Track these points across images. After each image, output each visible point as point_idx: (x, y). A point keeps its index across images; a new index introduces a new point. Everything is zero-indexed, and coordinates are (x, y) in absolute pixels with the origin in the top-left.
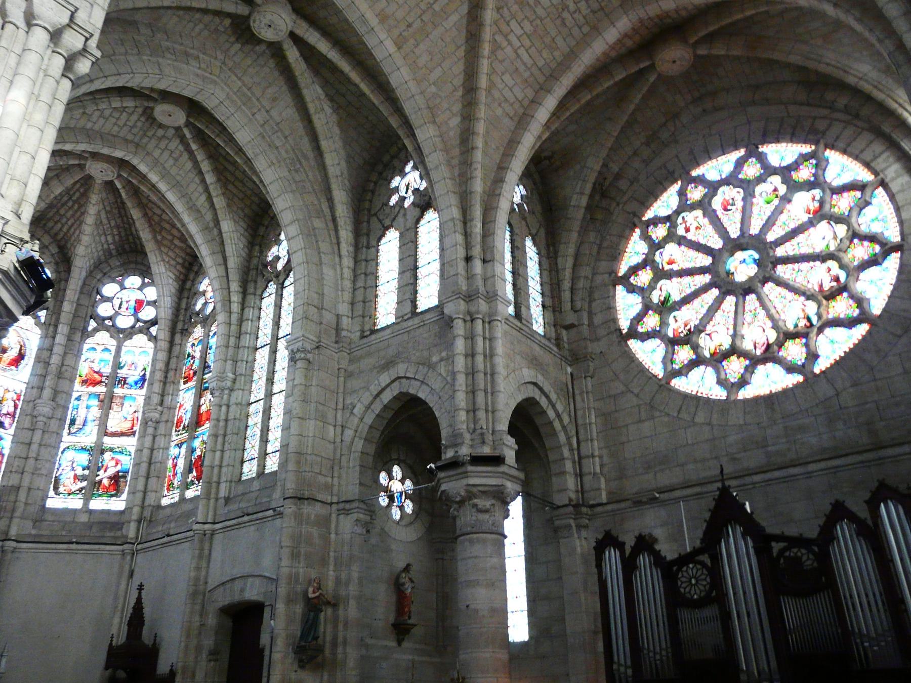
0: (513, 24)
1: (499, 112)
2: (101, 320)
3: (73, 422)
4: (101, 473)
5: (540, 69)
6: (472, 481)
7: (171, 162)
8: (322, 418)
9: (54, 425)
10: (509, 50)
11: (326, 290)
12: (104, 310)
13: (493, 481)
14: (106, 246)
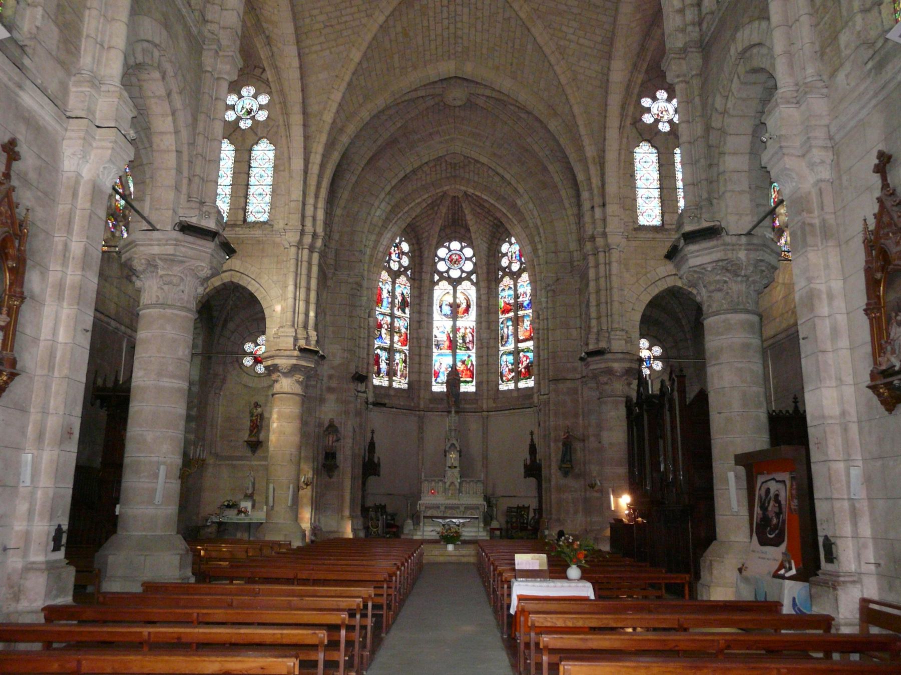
0: (564, 28)
3: (502, 337)
6: (595, 367)
7: (476, 176)
9: (492, 343)
10: (572, 46)
12: (505, 262)
13: (603, 366)
14: (491, 223)
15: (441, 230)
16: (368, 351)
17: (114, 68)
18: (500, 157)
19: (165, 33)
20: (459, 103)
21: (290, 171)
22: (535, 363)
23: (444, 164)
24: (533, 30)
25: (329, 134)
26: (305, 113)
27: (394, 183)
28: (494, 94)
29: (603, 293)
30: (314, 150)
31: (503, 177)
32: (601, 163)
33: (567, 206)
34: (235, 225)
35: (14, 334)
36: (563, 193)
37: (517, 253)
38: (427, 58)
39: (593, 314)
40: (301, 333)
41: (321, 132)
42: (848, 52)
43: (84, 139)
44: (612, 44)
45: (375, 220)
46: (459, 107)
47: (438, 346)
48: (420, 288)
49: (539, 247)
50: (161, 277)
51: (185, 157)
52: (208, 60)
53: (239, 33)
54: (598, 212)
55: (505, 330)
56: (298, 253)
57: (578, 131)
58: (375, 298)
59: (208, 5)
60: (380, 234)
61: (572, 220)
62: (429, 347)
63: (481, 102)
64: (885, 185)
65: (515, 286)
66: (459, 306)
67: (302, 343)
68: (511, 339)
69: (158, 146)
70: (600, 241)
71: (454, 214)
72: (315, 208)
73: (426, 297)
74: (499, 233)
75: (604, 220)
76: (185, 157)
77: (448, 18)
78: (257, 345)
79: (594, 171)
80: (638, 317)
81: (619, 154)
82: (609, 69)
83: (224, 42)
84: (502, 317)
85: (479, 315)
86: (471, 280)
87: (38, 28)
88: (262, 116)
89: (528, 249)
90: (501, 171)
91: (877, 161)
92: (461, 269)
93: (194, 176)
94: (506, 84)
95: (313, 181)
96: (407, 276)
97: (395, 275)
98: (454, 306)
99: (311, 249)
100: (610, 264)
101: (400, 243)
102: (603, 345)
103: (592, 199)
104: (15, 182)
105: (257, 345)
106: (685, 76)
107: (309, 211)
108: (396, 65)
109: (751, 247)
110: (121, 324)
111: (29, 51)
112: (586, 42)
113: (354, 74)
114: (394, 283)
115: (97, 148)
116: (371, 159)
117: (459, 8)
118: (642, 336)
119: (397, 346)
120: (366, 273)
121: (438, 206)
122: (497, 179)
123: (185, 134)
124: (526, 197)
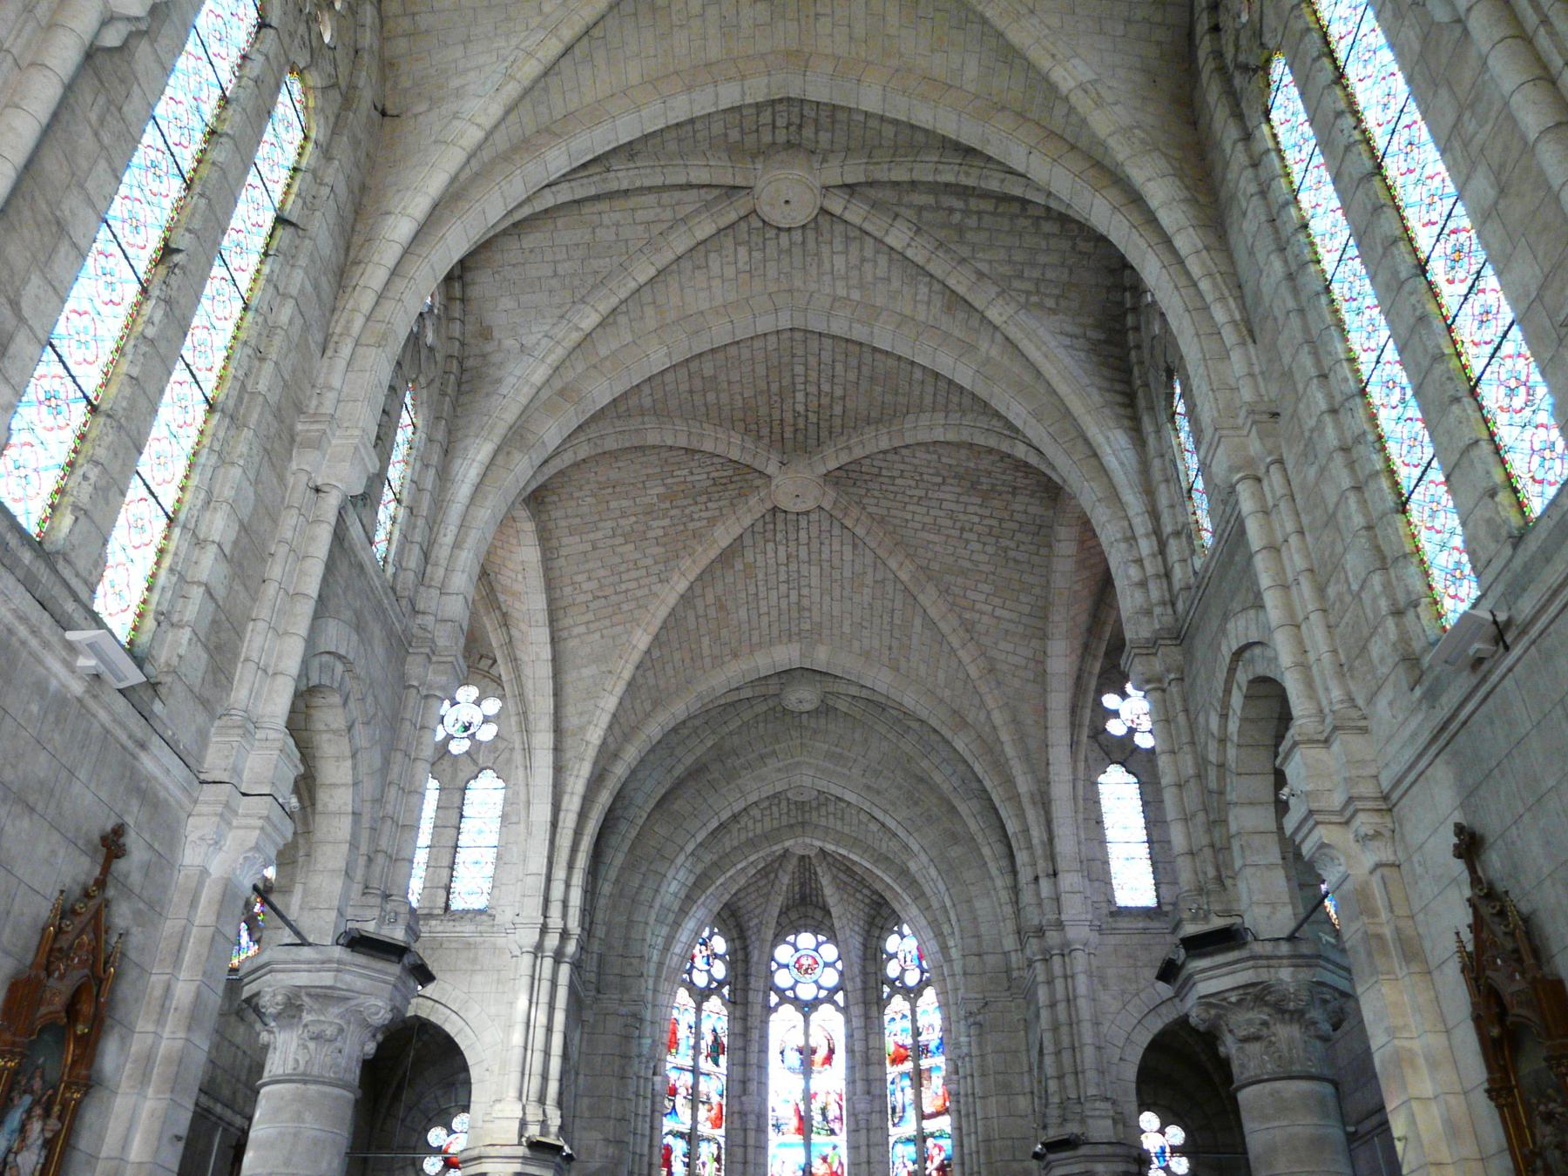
1: (1017, 683)
2: (891, 983)
3: (894, 1109)
4: (928, 1164)
7: (839, 823)
8: (1005, 1089)
9: (875, 1118)
10: (985, 619)
11: (983, 929)
12: (892, 970)
16: (651, 1140)
17: (279, 704)
19: (355, 637)
20: (807, 707)
21: (528, 825)
22: (956, 1160)
23: (784, 803)
24: (921, 598)
25: (595, 763)
26: (558, 730)
28: (865, 693)
29: (1064, 1030)
30: (569, 789)
31: (883, 825)
33: (994, 872)
35: (62, 1153)
36: (986, 851)
37: (915, 952)
38: (755, 639)
39: (1050, 1070)
40: (534, 1113)
42: (1385, 670)
43: (221, 815)
47: (777, 1127)
48: (745, 1019)
49: (951, 943)
50: (306, 1026)
51: (366, 822)
53: (465, 627)
54: (1045, 884)
55: (899, 1094)
58: (666, 1038)
59: (422, 589)
60: (677, 925)
61: (1004, 896)
62: (761, 1130)
63: (842, 705)
64: (1475, 881)
65: (913, 1012)
66: (814, 1052)
67: (533, 1131)
68: (911, 1114)
69: (325, 805)
70: (1053, 937)
71: (802, 885)
72: (568, 885)
73: (755, 1035)
74: (880, 917)
76: (366, 822)
77: (788, 582)
78: (451, 1131)
80: (1131, 1072)
83: (441, 642)
84: (892, 1071)
85: (851, 1068)
86: (835, 1003)
87: (180, 657)
88: (487, 733)
89: (932, 946)
91: (1455, 840)
92: (816, 982)
93: (377, 851)
94: (881, 680)
95: (565, 841)
96: (722, 997)
97: (701, 996)
98: (807, 1053)
99: (558, 957)
101: (710, 938)
102: (1073, 1128)
103: (1034, 864)
104: (111, 892)
105: (451, 1131)
106: (1160, 680)
107: (557, 891)
108: (706, 652)
109: (1299, 961)
110: (217, 1100)
111: (163, 690)
113: (637, 668)
114: (699, 1009)
115: (237, 828)
116: (664, 798)
117: (804, 569)
118: (1144, 1106)
119: (705, 1128)
120: (650, 993)
122: (874, 827)
123: (369, 787)
124: (924, 858)
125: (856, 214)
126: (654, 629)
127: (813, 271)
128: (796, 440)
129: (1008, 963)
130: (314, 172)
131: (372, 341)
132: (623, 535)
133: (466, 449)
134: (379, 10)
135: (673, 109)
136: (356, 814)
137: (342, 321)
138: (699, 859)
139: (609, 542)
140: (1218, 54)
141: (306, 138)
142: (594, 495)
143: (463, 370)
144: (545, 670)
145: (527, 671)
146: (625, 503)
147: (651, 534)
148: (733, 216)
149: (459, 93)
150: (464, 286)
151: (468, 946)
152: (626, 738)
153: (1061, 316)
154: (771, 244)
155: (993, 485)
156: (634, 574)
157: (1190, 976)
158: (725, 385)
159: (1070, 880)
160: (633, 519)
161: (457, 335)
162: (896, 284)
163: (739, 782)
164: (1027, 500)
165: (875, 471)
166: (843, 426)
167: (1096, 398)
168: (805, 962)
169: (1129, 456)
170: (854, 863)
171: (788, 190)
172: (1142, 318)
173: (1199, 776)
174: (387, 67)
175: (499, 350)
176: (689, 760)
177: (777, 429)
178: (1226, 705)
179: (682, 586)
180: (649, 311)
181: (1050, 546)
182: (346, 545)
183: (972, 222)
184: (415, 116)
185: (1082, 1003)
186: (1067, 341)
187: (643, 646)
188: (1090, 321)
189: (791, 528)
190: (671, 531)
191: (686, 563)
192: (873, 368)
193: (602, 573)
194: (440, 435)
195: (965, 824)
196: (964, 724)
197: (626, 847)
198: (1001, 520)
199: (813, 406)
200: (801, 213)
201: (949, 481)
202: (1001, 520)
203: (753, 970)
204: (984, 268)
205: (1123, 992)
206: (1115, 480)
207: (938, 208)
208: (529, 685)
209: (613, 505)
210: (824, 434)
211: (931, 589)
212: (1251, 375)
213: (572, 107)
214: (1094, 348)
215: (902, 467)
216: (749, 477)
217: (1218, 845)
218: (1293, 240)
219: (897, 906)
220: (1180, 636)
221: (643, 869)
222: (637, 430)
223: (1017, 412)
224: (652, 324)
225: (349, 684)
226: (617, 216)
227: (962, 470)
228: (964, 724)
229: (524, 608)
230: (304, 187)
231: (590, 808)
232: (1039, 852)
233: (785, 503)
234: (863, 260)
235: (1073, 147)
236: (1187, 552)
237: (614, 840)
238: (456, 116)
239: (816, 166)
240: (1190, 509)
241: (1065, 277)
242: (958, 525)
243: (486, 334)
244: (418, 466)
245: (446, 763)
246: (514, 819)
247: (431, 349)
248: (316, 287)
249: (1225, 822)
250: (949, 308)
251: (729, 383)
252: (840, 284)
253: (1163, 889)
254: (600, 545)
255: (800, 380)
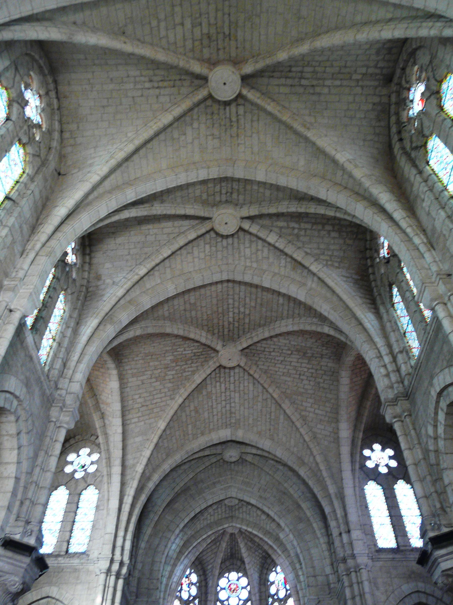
0: (304, 403)
1: (326, 443)
5: (330, 412)
10: (311, 415)
11: (316, 563)
12: (273, 590)
15: (222, 563)
18: (265, 499)
19: (24, 390)
20: (233, 459)
21: (108, 510)
24: (283, 405)
25: (140, 481)
27: (186, 521)
28: (259, 452)
30: (127, 493)
31: (268, 515)
32: (342, 498)
33: (319, 535)
34: (58, 556)
36: (315, 525)
38: (211, 427)
41: (134, 479)
44: (337, 413)
45: (171, 553)
46: (234, 462)
49: (300, 573)
51: (22, 483)
52: (54, 413)
54: (345, 536)
56: (106, 580)
57: (321, 475)
60: (174, 565)
61: (324, 547)
63: (249, 458)
70: (350, 562)
71: (231, 549)
72: (124, 540)
74: (267, 564)
75: (351, 544)
76: (22, 483)
77: (225, 400)
79: (336, 504)
81: (355, 490)
82: (338, 429)
88: (92, 469)
89: (291, 576)
90: (266, 510)
93: (26, 499)
94: (266, 444)
95: (124, 518)
100: (362, 582)
103: (339, 527)
106: (400, 417)
107: (119, 542)
108: (190, 432)
112: (320, 412)
121: (220, 541)
122: (264, 517)
123: (25, 465)
124: (287, 530)
125: (254, 229)
126: (167, 420)
127: (237, 255)
128: (229, 336)
129: (328, 581)
130: (26, 185)
131: (44, 254)
132: (156, 378)
133: (86, 322)
134: (61, 136)
135: (179, 178)
136: (17, 479)
137: (31, 245)
138: (186, 533)
139: (149, 381)
140: (403, 148)
141: (24, 172)
142: (143, 359)
143: (88, 292)
144: (119, 438)
145: (111, 439)
146: (156, 363)
147: (167, 378)
148: (203, 230)
149: (91, 165)
150: (91, 259)
151: (75, 570)
152: (154, 470)
153: (340, 270)
154: (219, 244)
155: (313, 354)
156: (159, 396)
157: (436, 559)
158: (199, 308)
159: (356, 534)
160: (159, 370)
161: (86, 277)
162: (271, 260)
163: (204, 494)
164: (327, 360)
165: (263, 349)
166: (249, 329)
167: (359, 301)
168: (233, 587)
169: (375, 323)
170: (256, 536)
171: (227, 219)
172: (376, 269)
173: (424, 459)
174: (62, 157)
175: (104, 284)
176: (182, 484)
177: (221, 330)
178: (436, 420)
179: (180, 401)
180: (168, 271)
181: (338, 381)
182: (24, 345)
183: (302, 233)
184: (72, 174)
185: (368, 596)
186: (345, 279)
187: (163, 427)
188: (353, 272)
189: (227, 376)
190: (176, 376)
191: (182, 390)
192: (262, 299)
193: (145, 395)
194: (75, 315)
195: (305, 513)
196: (303, 463)
197: (152, 525)
198: (316, 370)
199: (237, 318)
200: (231, 229)
201: (294, 353)
202: (316, 370)
203: (209, 590)
204: (309, 251)
205: (386, 591)
206: (370, 333)
207: (288, 227)
208: (111, 445)
209: (151, 364)
210: (241, 332)
211: (287, 401)
212: (435, 261)
213: (138, 175)
214: (356, 282)
215: (274, 347)
216: (209, 352)
217: (439, 491)
218: (448, 203)
219: (274, 557)
220: (408, 395)
221: (160, 535)
222: (161, 326)
223: (324, 308)
224: (169, 276)
225: (20, 412)
226: (155, 231)
227: (299, 347)
228: (303, 463)
229: (111, 410)
230: (20, 188)
231: (136, 503)
232: (341, 521)
233: (225, 363)
234: (257, 250)
235: (346, 188)
236: (407, 359)
237: (147, 522)
238: (89, 172)
239: (238, 209)
240: (406, 341)
241: (342, 254)
242: (298, 373)
243: (98, 278)
244: (64, 326)
245: (73, 482)
246: (102, 508)
247: (74, 280)
248: (21, 227)
249: (441, 479)
250: (294, 269)
251: (201, 307)
252: (248, 261)
253: (399, 539)
254: (145, 382)
255: (231, 306)
